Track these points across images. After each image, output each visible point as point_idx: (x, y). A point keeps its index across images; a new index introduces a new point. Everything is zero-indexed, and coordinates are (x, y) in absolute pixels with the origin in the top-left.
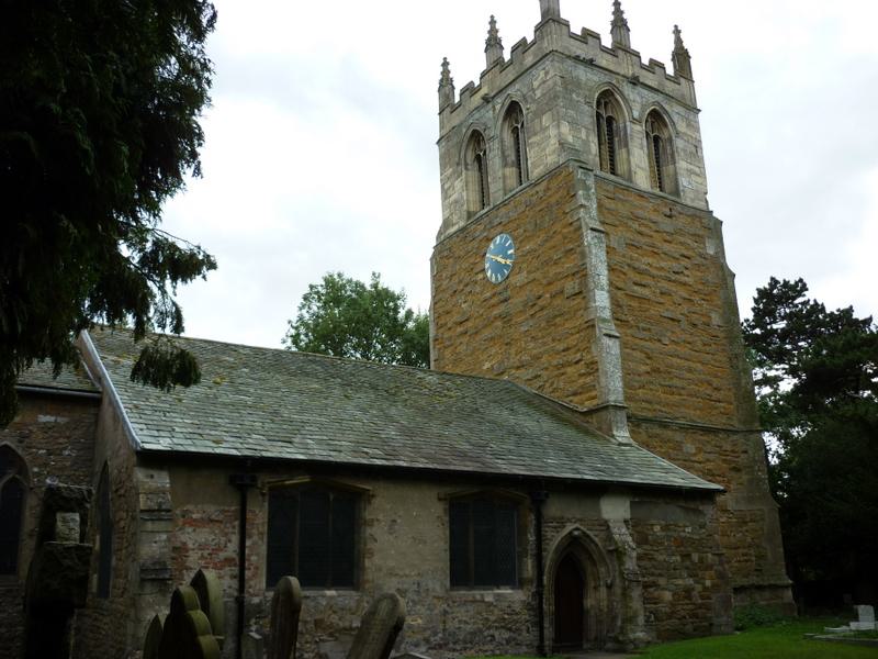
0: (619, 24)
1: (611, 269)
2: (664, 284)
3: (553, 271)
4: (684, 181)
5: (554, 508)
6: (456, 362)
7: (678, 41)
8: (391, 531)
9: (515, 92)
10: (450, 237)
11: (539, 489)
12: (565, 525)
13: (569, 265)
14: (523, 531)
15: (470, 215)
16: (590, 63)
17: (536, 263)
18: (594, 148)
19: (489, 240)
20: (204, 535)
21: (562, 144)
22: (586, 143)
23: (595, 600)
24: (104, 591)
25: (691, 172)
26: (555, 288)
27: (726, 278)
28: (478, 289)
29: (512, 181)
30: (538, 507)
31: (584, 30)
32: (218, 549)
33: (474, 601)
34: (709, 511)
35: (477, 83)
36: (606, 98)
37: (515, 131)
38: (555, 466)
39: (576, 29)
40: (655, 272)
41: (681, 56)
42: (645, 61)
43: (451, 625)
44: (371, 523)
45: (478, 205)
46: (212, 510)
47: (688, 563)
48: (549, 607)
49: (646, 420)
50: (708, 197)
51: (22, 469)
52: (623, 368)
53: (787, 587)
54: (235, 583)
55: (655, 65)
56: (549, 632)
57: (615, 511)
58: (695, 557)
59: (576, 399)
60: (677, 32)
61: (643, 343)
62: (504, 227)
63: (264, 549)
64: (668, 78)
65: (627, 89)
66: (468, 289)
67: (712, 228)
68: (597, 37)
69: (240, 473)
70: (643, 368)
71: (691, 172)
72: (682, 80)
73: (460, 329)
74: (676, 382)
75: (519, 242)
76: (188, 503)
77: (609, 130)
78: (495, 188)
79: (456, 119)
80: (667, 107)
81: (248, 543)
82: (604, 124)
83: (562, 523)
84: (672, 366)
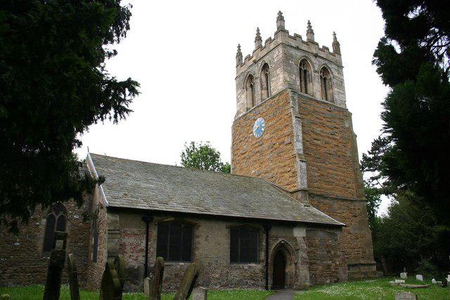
0: (310, 32)
1: (303, 133)
2: (326, 139)
3: (280, 133)
4: (336, 97)
5: (273, 232)
6: (241, 169)
7: (335, 38)
8: (206, 240)
9: (266, 60)
10: (240, 118)
11: (268, 224)
12: (278, 238)
13: (286, 131)
14: (261, 242)
15: (247, 109)
16: (297, 48)
17: (272, 131)
18: (298, 83)
19: (255, 120)
20: (132, 240)
21: (285, 81)
22: (295, 81)
23: (290, 269)
24: (95, 260)
25: (339, 93)
26: (280, 141)
27: (352, 138)
28: (250, 140)
29: (265, 96)
30: (267, 231)
31: (295, 34)
32: (137, 246)
33: (240, 268)
34: (339, 233)
35: (251, 55)
36: (304, 62)
37: (266, 75)
38: (276, 215)
39: (292, 34)
40: (322, 134)
41: (336, 45)
42: (321, 47)
43: (230, 278)
44: (198, 237)
45: (251, 105)
46: (135, 230)
47: (329, 255)
48: (270, 272)
49: (318, 195)
50: (346, 103)
51: (65, 212)
52: (308, 174)
53: (373, 265)
54: (144, 259)
55: (325, 48)
56: (270, 282)
57: (299, 233)
58: (333, 253)
59: (288, 187)
60: (335, 34)
61: (317, 164)
62: (261, 115)
63: (155, 246)
64: (330, 53)
65: (313, 58)
66: (246, 140)
67: (347, 116)
68: (300, 37)
69: (147, 216)
70: (316, 174)
71: (339, 93)
72: (336, 55)
73: (243, 156)
74: (331, 180)
75: (267, 121)
76: (126, 227)
77: (304, 75)
78: (258, 98)
79: (243, 69)
80: (329, 66)
81: (149, 243)
82: (303, 74)
83: (277, 238)
84: (329, 173)
